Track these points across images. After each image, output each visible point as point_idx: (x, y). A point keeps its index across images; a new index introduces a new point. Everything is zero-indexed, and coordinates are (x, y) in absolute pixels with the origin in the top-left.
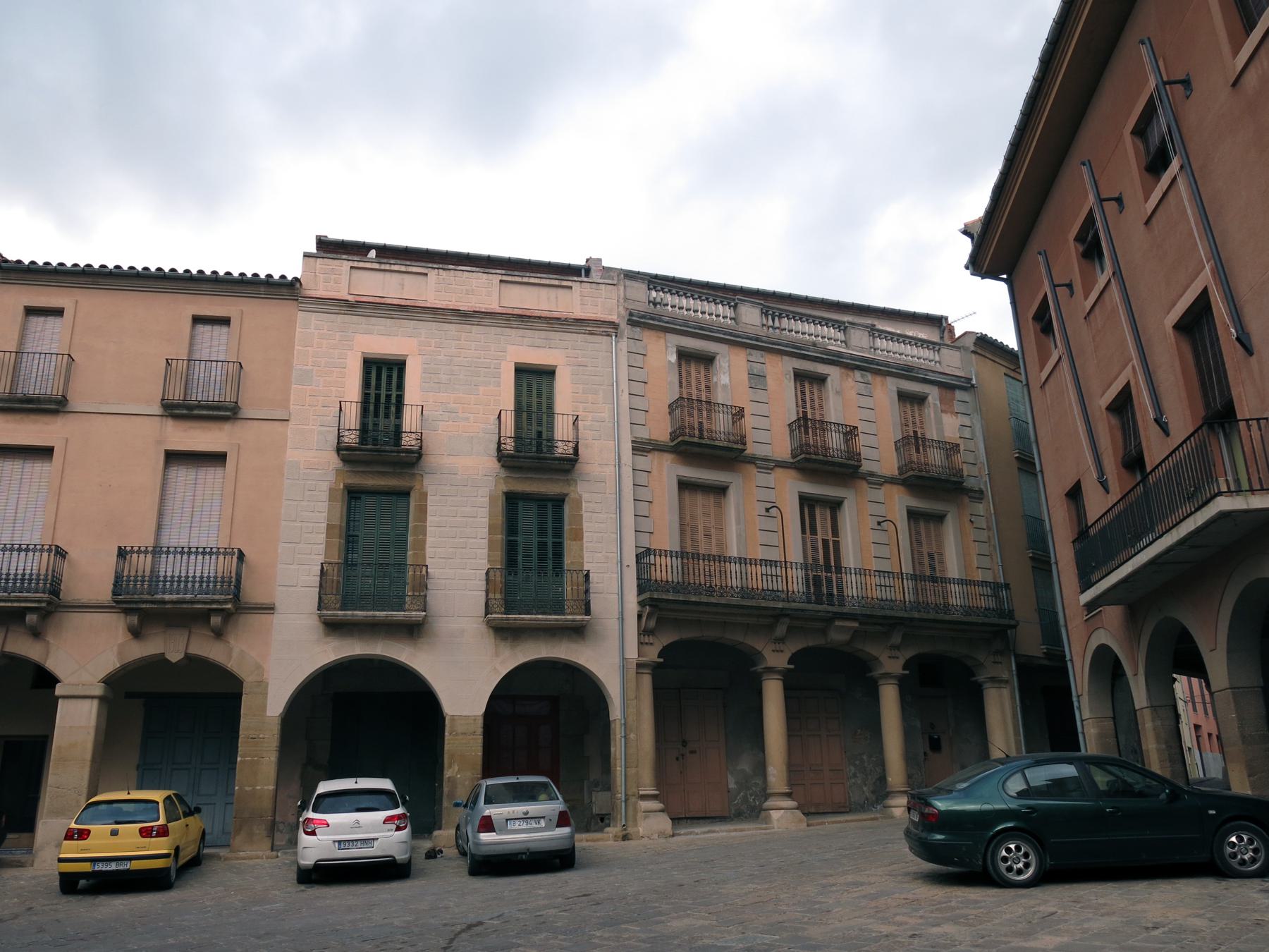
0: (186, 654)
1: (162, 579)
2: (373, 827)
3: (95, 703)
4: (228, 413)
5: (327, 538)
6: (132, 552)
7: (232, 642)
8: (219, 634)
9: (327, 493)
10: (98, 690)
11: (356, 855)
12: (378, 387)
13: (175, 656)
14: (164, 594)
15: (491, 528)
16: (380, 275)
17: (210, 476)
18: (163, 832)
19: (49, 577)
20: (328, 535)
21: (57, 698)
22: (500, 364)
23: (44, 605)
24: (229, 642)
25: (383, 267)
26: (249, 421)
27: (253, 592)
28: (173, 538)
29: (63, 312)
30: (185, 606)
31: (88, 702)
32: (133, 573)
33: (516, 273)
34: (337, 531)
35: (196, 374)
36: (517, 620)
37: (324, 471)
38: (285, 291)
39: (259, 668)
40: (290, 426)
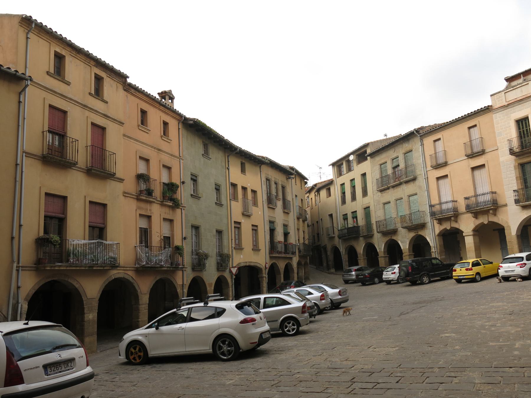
0: (451, 227)
2: (513, 267)
4: (482, 153)
5: (517, 181)
6: (470, 197)
7: (499, 216)
9: (514, 167)
10: (471, 233)
11: (510, 274)
12: (523, 128)
13: (448, 228)
14: (481, 207)
16: (514, 91)
17: (483, 171)
18: (471, 269)
23: (453, 215)
27: (501, 202)
28: (444, 200)
30: (482, 210)
31: (470, 236)
34: (519, 178)
35: (473, 143)
37: (511, 161)
39: (507, 222)
40: (499, 151)
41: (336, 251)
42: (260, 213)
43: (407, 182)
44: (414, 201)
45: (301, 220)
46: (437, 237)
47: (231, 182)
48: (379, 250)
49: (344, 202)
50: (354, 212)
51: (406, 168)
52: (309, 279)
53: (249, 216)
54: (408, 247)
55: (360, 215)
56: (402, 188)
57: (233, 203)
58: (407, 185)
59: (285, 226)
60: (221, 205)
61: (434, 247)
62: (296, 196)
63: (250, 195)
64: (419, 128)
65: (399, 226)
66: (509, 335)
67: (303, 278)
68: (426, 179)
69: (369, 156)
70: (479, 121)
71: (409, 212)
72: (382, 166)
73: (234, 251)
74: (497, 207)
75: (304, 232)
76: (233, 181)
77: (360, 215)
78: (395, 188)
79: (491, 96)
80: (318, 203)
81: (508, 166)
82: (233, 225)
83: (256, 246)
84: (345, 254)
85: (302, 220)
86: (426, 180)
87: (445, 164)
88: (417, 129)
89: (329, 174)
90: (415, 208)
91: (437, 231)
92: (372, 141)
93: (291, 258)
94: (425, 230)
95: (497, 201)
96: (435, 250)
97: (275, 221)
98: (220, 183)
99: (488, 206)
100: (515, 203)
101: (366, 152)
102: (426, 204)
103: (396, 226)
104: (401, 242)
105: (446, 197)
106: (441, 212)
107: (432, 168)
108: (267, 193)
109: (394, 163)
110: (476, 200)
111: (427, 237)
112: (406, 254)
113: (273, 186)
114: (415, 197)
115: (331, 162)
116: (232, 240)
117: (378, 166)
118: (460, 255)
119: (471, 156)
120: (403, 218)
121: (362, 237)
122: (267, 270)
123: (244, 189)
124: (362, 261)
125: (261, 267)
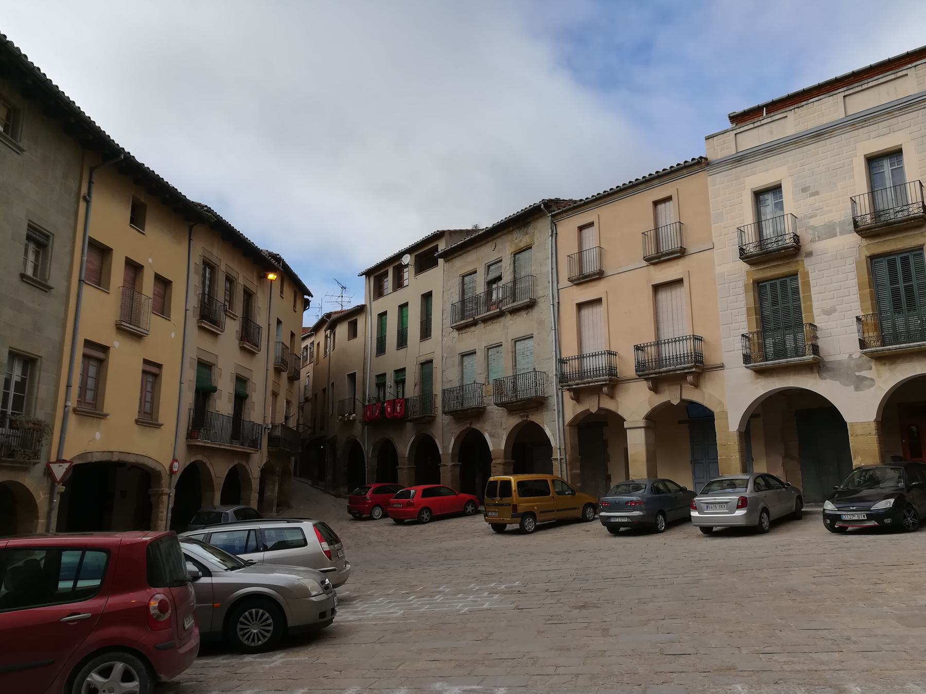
1: (664, 358)
3: (643, 430)
4: (679, 254)
8: (696, 385)
10: (642, 424)
13: (594, 410)
14: (670, 366)
15: (860, 286)
19: (693, 354)
20: (748, 315)
21: (626, 429)
22: (741, 193)
23: (608, 382)
24: (702, 390)
25: (756, 125)
26: (691, 255)
27: (711, 358)
29: (672, 197)
30: (671, 373)
31: (639, 430)
32: (650, 358)
33: (856, 85)
34: (753, 311)
36: (890, 350)
37: (739, 275)
38: (685, 172)
39: (721, 403)
41: (355, 448)
42: (173, 335)
43: (514, 311)
44: (526, 351)
45: (284, 375)
46: (567, 428)
47: (90, 238)
48: (443, 451)
49: (381, 348)
50: (401, 372)
51: (515, 281)
52: (289, 506)
53: (138, 337)
54: (503, 447)
55: (412, 377)
56: (502, 324)
57: (89, 293)
58: (515, 317)
59: (241, 381)
60: (45, 288)
61: (560, 449)
62: (279, 322)
63: (148, 286)
64: (551, 200)
65: (490, 402)
66: (788, 688)
67: (275, 502)
68: (556, 305)
69: (441, 256)
70: (677, 189)
71: (513, 373)
72: (466, 279)
73: (72, 419)
74: (703, 370)
75: (288, 402)
76: (98, 233)
77: (412, 377)
78: (489, 323)
79: (707, 138)
80: (330, 353)
81: (731, 284)
82: (80, 350)
83: (151, 414)
84: (372, 457)
85: (288, 377)
86: (556, 308)
87: (599, 275)
88: (548, 200)
89: (358, 295)
90: (525, 367)
91: (569, 416)
92: (452, 229)
93: (247, 456)
94: (544, 413)
95: (702, 357)
96: (560, 456)
97: (214, 365)
98: (48, 227)
99: (687, 365)
100: (744, 363)
101: (436, 249)
102: (550, 357)
103: (482, 402)
104: (491, 436)
105: (595, 343)
106: (581, 374)
107: (570, 284)
108: (204, 294)
109: (490, 273)
110: (659, 353)
111: (546, 426)
112: (500, 461)
113: (221, 284)
114: (529, 343)
115: (364, 269)
116: (68, 386)
117: (458, 280)
118: (607, 470)
119: (657, 259)
120: (499, 384)
121: (410, 421)
122: (176, 479)
123: (134, 268)
124: (405, 472)
125: (159, 468)
